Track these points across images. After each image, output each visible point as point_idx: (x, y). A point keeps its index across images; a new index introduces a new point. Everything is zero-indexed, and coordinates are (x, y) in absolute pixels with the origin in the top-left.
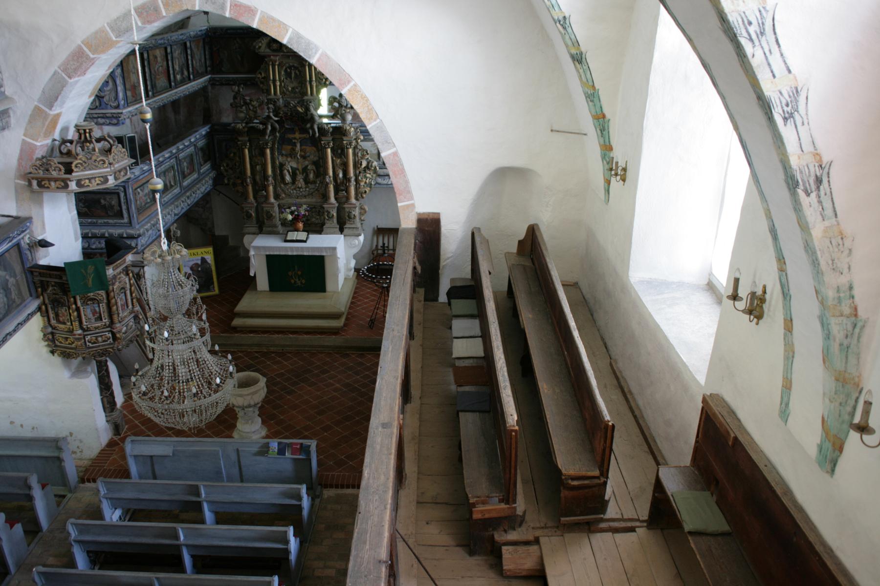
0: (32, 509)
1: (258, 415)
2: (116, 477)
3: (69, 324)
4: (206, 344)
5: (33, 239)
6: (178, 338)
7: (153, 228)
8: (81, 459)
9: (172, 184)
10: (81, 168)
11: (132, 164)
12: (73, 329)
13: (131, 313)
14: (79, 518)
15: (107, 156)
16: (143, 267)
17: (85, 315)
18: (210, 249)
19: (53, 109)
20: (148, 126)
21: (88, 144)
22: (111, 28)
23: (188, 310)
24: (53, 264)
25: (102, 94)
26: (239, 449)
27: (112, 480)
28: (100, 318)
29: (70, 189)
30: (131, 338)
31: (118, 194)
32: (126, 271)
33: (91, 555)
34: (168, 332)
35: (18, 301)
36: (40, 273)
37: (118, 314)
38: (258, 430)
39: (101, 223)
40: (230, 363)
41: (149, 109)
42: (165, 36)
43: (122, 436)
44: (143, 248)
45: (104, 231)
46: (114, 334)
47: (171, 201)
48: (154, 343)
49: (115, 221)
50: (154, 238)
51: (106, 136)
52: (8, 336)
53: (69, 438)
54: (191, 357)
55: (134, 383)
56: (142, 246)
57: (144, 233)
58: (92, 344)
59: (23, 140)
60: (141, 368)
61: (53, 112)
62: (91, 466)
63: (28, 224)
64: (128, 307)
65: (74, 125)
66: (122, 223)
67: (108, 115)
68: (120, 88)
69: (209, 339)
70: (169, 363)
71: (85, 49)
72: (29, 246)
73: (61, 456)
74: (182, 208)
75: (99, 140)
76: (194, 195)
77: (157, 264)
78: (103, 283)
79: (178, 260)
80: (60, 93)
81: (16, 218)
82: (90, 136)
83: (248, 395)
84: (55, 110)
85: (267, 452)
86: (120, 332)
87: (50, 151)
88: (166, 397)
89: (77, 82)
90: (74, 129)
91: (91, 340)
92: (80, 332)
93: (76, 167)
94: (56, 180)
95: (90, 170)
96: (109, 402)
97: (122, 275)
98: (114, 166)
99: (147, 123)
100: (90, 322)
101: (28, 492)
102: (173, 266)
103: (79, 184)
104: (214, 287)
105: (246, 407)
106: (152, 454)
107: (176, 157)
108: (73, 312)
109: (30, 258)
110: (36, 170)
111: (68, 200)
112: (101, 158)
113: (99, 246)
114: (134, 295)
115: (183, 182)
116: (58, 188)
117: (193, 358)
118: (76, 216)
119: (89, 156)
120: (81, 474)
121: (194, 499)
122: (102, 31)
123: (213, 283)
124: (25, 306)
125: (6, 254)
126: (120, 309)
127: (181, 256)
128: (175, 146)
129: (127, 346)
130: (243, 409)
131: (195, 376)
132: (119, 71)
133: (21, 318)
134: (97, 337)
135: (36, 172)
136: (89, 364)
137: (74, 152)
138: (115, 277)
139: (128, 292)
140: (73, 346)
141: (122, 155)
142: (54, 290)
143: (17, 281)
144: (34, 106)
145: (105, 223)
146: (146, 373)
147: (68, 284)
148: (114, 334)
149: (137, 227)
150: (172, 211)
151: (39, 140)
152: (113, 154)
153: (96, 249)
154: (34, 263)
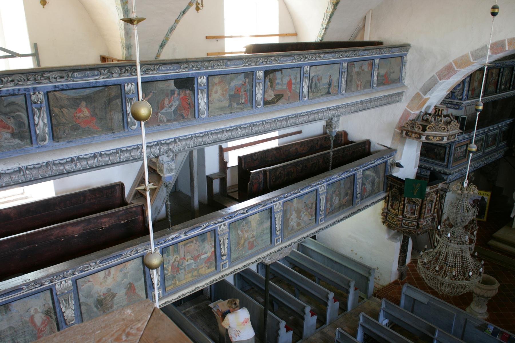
0: (347, 298)
1: (487, 305)
2: (392, 302)
3: (397, 211)
4: (471, 249)
5: (394, 161)
6: (455, 240)
7: (459, 172)
8: (378, 284)
9: (479, 149)
10: (431, 130)
11: (459, 134)
12: (398, 214)
13: (431, 216)
14: (366, 314)
15: (447, 126)
16: (446, 192)
17: (407, 209)
18: (489, 193)
19: (426, 95)
20: (478, 114)
21: (439, 117)
22: (472, 55)
23: (467, 225)
24: (399, 177)
25: (455, 91)
26: (468, 319)
27: (390, 302)
28: (414, 213)
29: (421, 139)
30: (427, 229)
31: (446, 148)
32: (437, 192)
33: (365, 336)
34: (450, 234)
35: (376, 191)
36: (392, 180)
37: (424, 214)
38: (483, 313)
39: (431, 162)
40: (482, 266)
41: (482, 104)
42: (502, 62)
43: (403, 281)
44: (450, 181)
45: (431, 166)
46: (418, 224)
47: (475, 159)
48: (440, 238)
49: (439, 162)
50: (458, 178)
51: (450, 114)
52: (366, 207)
53: (376, 270)
54: (459, 254)
55: (421, 255)
56: (450, 180)
57: (453, 173)
58: (405, 225)
59: (406, 109)
60: (428, 248)
61: (425, 97)
62: (381, 289)
63: (394, 153)
64: (431, 212)
65: (434, 106)
66: (443, 165)
67: (454, 103)
68: (466, 89)
69: (473, 247)
70: (445, 252)
71: (454, 65)
72: (391, 164)
73: (369, 278)
74: (480, 165)
75: (445, 116)
76: (490, 159)
77: (458, 194)
78: (422, 195)
79: (471, 195)
80: (433, 87)
81: (389, 148)
82: (441, 113)
83: (485, 289)
84: (427, 96)
85: (485, 330)
86: (422, 224)
87: (418, 116)
88: (436, 270)
89: (443, 82)
90: (434, 107)
91: (406, 223)
92: (401, 217)
93: (429, 128)
94: (416, 133)
95: (436, 131)
96: (402, 260)
97: (434, 194)
98: (449, 132)
99: (478, 111)
100: (408, 213)
101: (348, 289)
102: (467, 197)
103: (427, 138)
104: (484, 217)
105: (481, 296)
106: (416, 298)
107: (486, 134)
108: (401, 205)
109: (389, 171)
110: (407, 126)
111: (418, 145)
112: (444, 126)
113: (426, 174)
114: (436, 206)
115: (486, 149)
116: (415, 138)
117: (460, 255)
118: (419, 155)
119: (437, 124)
120: (376, 292)
121: (430, 335)
122: (466, 56)
123: (484, 214)
124: (379, 195)
125: (379, 166)
126: (426, 211)
127: (474, 193)
128: (488, 128)
129: (423, 234)
130: (478, 297)
131: (457, 265)
132: (468, 79)
133: (375, 200)
134: (409, 223)
135: (407, 127)
136: (399, 235)
137: (430, 120)
138: (429, 193)
139: (434, 204)
140: (395, 223)
141: (456, 127)
142: (396, 190)
143: (379, 180)
144: (416, 92)
145: (433, 162)
146: (430, 252)
147: (404, 190)
148: (418, 224)
149: (451, 169)
150: (474, 165)
151: (414, 110)
152: (451, 125)
153: (424, 175)
154: (390, 173)
